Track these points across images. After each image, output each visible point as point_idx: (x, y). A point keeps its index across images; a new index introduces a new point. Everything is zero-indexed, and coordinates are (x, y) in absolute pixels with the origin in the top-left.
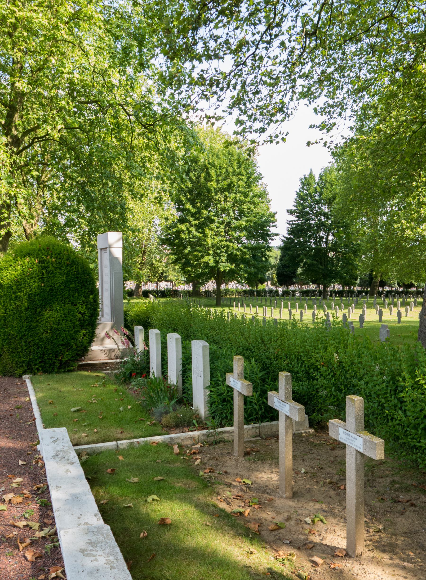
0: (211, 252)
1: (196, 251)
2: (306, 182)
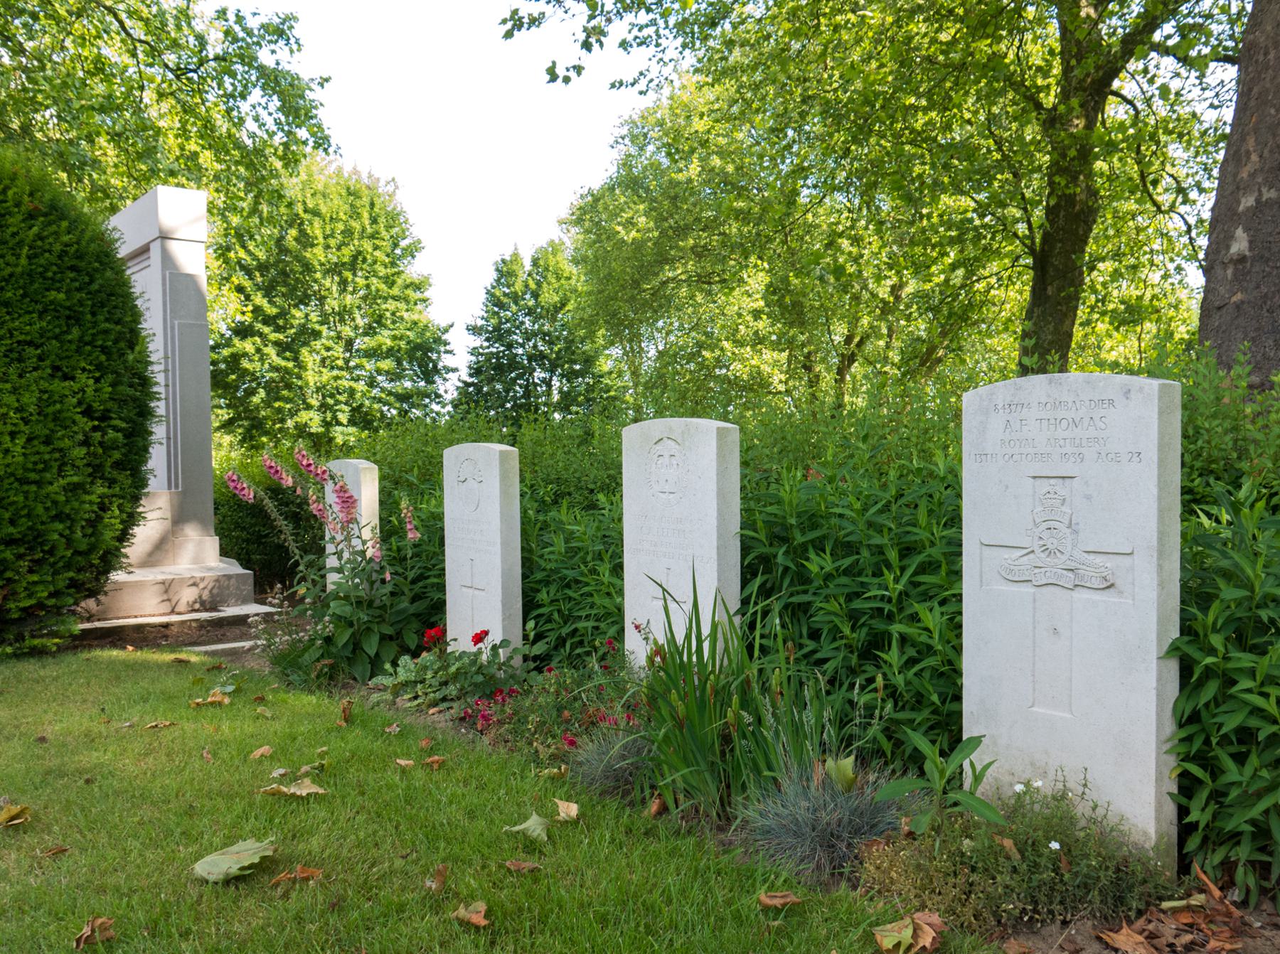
0: (315, 402)
1: (278, 399)
2: (505, 272)
